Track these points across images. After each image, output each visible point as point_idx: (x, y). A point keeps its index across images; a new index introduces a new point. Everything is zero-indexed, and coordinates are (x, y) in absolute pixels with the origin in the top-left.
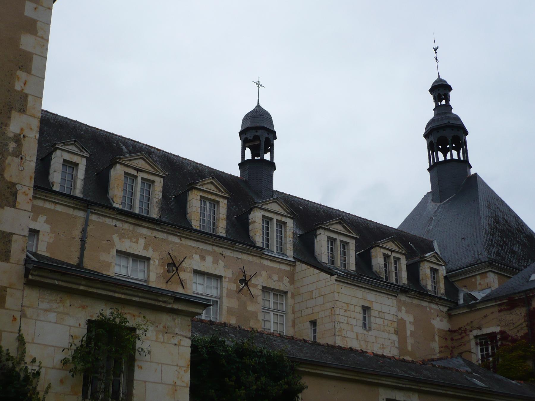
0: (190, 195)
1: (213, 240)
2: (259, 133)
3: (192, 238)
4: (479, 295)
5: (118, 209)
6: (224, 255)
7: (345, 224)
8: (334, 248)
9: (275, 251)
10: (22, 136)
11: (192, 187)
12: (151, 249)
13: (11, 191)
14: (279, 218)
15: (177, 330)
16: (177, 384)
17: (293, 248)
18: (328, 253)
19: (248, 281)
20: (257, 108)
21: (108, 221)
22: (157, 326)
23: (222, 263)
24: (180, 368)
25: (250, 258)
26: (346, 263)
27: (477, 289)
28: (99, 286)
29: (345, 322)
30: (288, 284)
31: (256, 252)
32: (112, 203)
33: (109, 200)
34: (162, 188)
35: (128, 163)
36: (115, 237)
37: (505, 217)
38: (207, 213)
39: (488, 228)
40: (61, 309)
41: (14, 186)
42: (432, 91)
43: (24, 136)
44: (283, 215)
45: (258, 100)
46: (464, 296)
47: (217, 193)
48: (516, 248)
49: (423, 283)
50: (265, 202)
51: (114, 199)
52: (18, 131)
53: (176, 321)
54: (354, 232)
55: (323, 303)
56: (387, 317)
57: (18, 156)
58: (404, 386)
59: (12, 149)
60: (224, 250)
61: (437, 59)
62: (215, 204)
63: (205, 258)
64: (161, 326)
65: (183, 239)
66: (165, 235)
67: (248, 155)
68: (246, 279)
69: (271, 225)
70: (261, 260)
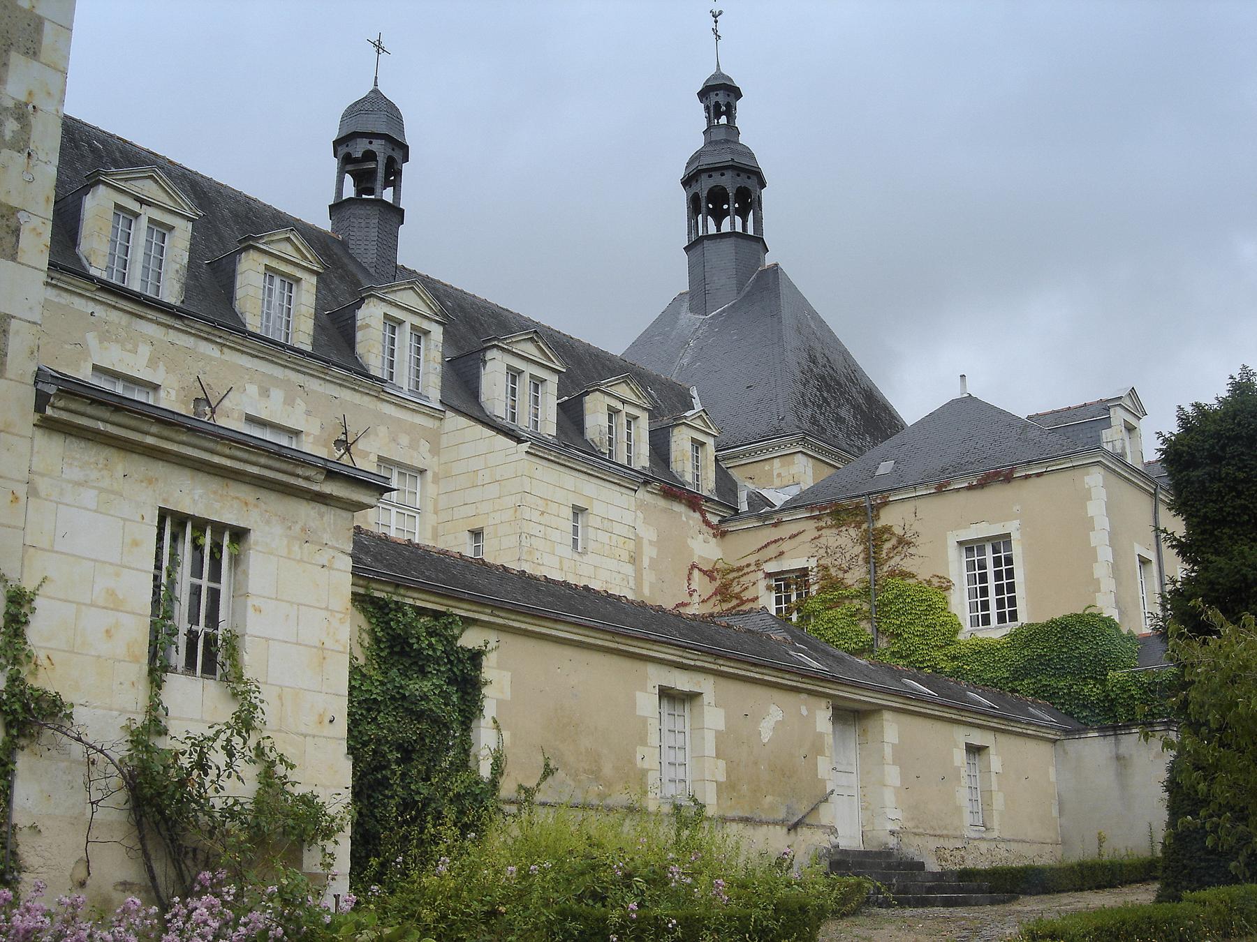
0: (243, 261)
1: (286, 358)
2: (377, 146)
3: (245, 350)
4: (778, 498)
5: (100, 281)
6: (306, 389)
7: (542, 343)
8: (517, 388)
9: (406, 388)
10: (30, 107)
11: (248, 245)
12: (162, 368)
13: (7, 226)
14: (417, 321)
15: (326, 538)
16: (326, 645)
17: (440, 384)
18: (507, 398)
19: (352, 444)
20: (372, 95)
21: (79, 303)
22: (290, 528)
23: (303, 404)
24: (331, 615)
25: (356, 398)
26: (539, 420)
27: (773, 485)
28: (184, 438)
29: (540, 535)
30: (428, 455)
31: (370, 387)
32: (88, 266)
33: (80, 259)
34: (189, 243)
35: (121, 185)
36: (92, 339)
37: (826, 352)
38: (275, 300)
39: (797, 372)
40: (106, 483)
41: (13, 214)
42: (703, 94)
43: (34, 107)
44: (426, 317)
45: (376, 78)
46: (749, 497)
47: (298, 261)
48: (843, 413)
49: (675, 467)
50: (392, 286)
51: (92, 259)
52: (23, 98)
53: (325, 519)
54: (558, 361)
55: (498, 496)
56: (618, 529)
57: (23, 150)
58: (692, 663)
59: (12, 135)
60: (307, 377)
61: (718, 34)
62: (292, 285)
63: (269, 391)
64: (297, 528)
65: (225, 350)
66: (192, 339)
67: (349, 191)
68: (347, 441)
69: (399, 334)
70: (378, 402)
